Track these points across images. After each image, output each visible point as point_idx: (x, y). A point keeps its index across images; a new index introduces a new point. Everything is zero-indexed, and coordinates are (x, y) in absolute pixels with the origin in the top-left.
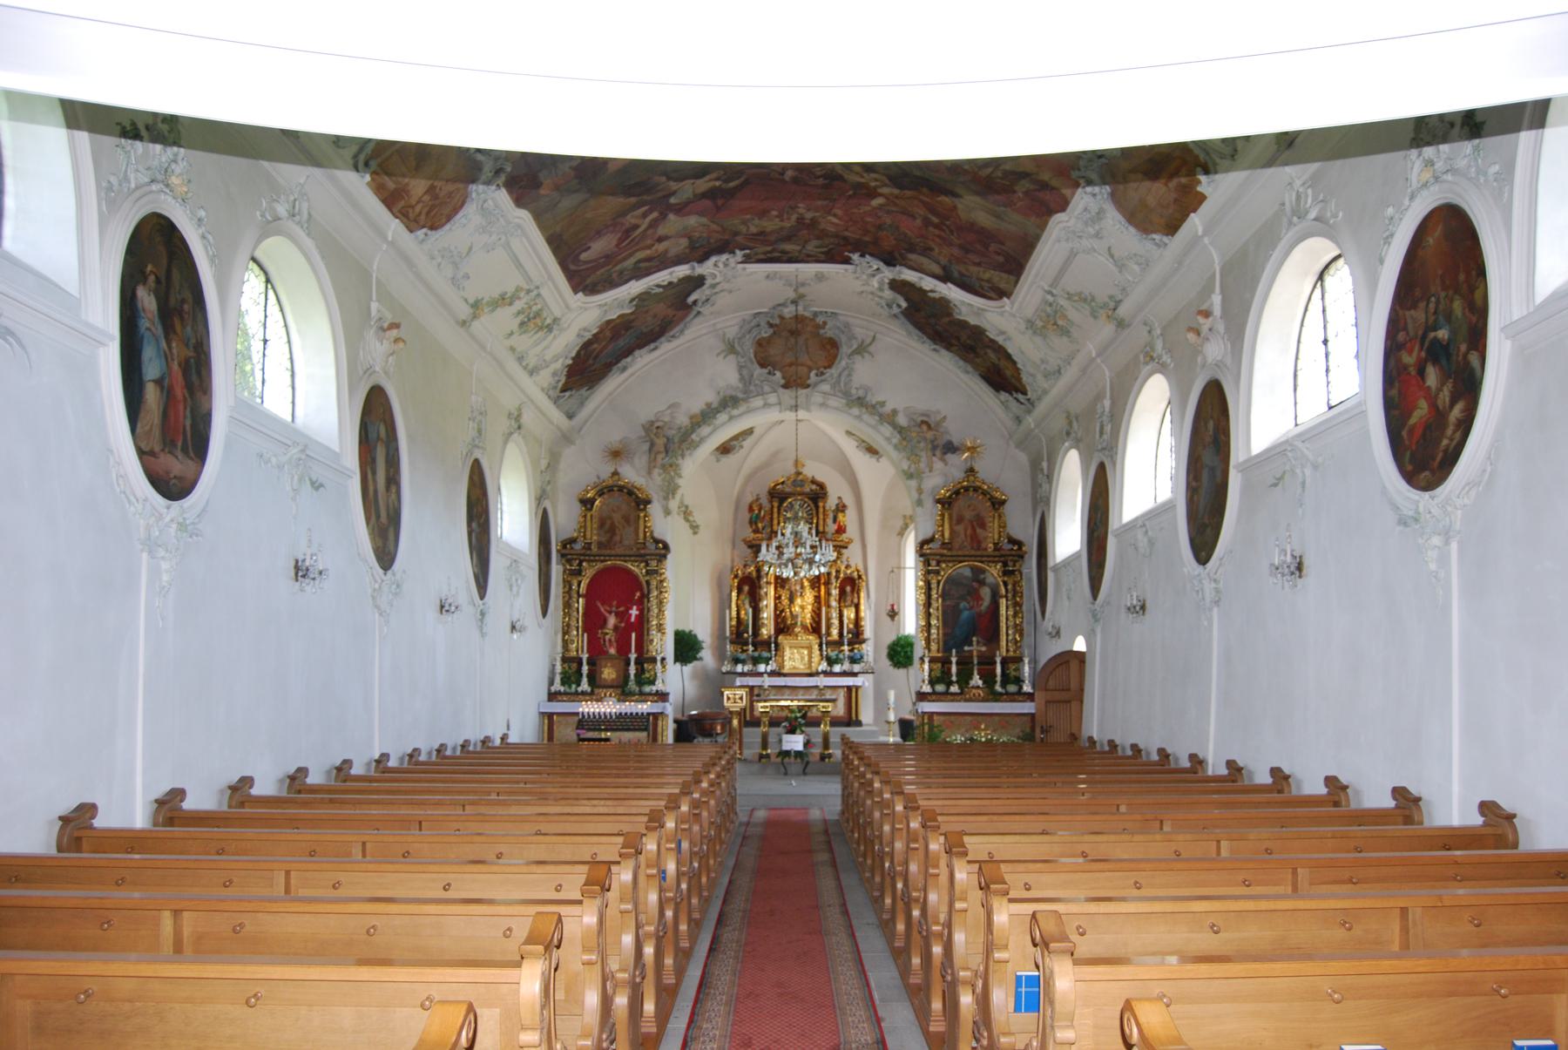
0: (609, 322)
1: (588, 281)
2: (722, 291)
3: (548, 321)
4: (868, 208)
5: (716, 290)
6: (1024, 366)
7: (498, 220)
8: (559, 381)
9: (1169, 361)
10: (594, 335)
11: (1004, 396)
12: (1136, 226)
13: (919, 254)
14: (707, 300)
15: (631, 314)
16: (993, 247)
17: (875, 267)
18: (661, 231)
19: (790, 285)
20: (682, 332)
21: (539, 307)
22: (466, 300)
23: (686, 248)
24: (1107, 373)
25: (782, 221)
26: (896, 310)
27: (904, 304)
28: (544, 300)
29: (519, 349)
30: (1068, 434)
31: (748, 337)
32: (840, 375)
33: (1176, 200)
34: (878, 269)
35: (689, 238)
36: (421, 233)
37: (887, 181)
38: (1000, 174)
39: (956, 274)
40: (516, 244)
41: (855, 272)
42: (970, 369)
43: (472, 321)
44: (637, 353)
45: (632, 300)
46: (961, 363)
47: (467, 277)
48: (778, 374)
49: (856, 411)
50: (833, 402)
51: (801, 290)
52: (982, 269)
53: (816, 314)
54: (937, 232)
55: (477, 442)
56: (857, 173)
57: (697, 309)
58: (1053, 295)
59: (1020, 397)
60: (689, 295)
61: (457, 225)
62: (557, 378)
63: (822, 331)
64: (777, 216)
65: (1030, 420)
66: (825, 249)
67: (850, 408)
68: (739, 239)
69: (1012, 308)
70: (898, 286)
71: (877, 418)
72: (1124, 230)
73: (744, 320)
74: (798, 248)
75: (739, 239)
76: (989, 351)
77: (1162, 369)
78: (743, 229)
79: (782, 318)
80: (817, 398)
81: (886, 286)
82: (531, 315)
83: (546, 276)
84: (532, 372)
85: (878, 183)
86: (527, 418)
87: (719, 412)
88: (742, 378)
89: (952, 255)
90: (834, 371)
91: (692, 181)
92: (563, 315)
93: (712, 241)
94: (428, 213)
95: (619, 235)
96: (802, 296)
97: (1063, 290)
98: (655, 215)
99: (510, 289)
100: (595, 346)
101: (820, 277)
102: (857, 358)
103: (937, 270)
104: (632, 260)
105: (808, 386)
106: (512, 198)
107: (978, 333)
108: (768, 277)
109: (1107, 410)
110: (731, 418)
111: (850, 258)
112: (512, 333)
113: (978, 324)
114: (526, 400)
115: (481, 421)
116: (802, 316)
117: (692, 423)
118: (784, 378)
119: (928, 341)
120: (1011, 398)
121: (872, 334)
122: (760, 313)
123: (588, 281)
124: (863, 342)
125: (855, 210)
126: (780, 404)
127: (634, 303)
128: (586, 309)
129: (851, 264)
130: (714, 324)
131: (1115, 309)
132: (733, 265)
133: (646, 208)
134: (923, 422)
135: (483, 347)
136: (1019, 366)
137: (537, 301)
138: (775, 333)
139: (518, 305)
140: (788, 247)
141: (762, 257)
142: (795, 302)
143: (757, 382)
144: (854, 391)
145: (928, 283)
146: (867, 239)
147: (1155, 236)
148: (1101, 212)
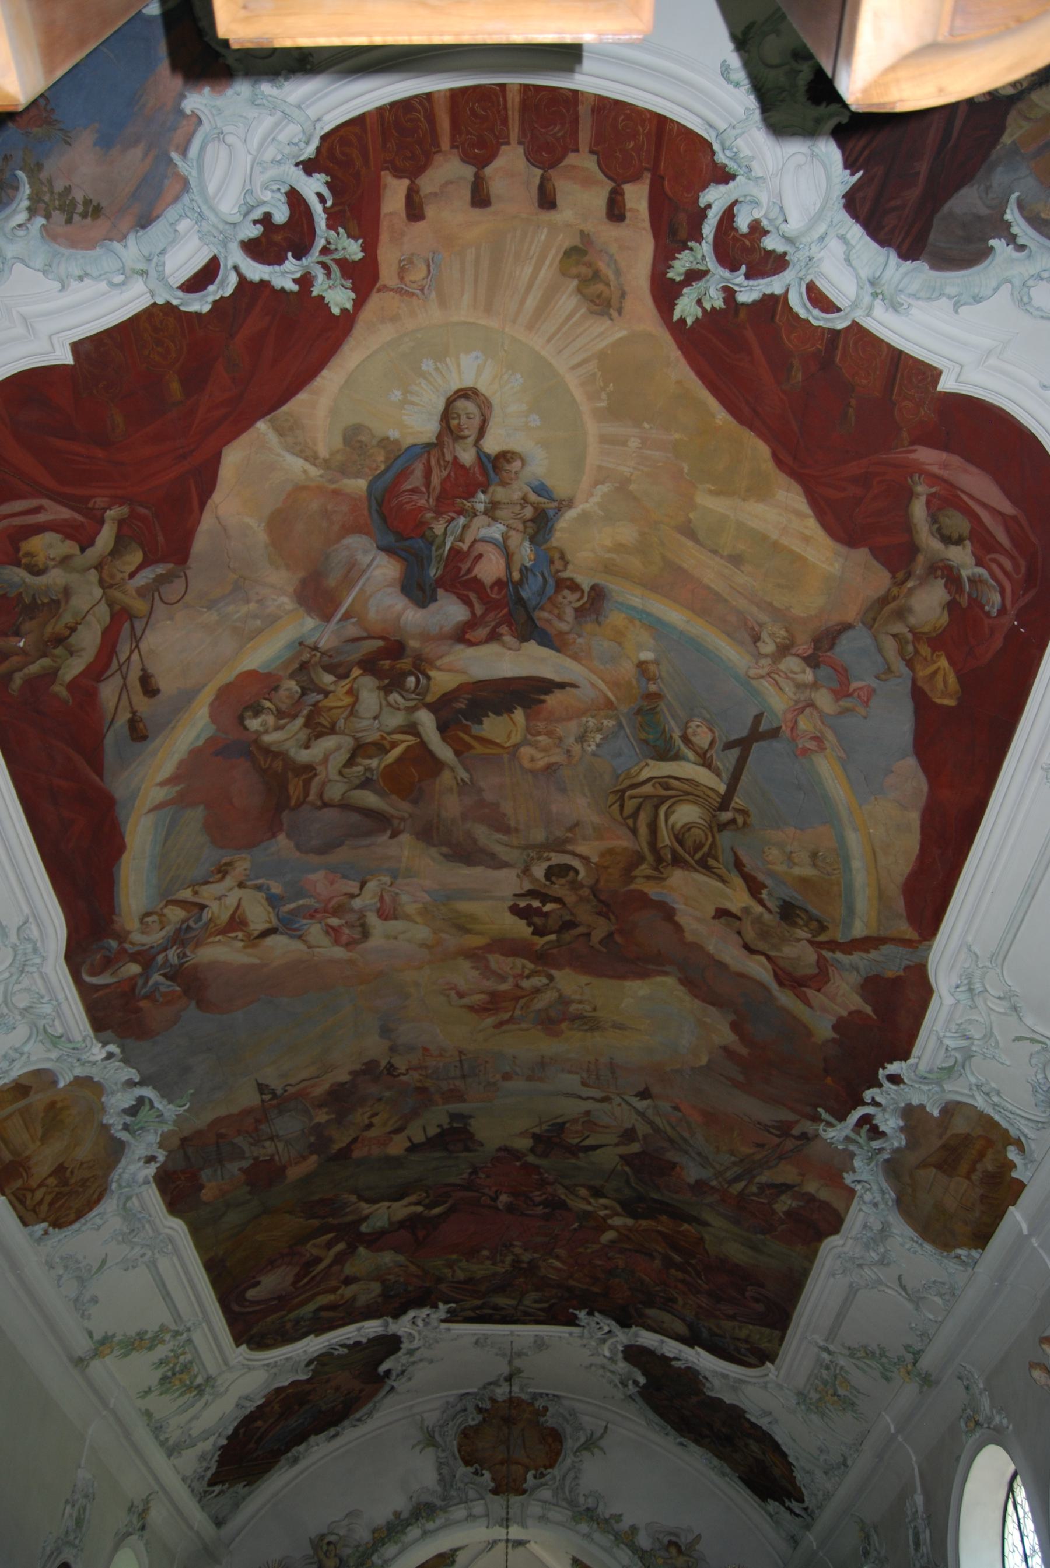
0: (279, 1390)
1: (254, 1330)
2: (421, 1360)
3: (199, 1380)
4: (596, 1247)
5: (412, 1359)
6: (797, 1459)
7: (144, 1227)
8: (208, 1468)
9: (1005, 1421)
10: (259, 1407)
11: (773, 1506)
12: (933, 1242)
13: (660, 1308)
14: (403, 1372)
15: (308, 1381)
17: (606, 1329)
18: (349, 1269)
19: (504, 1355)
20: (370, 1414)
21: (189, 1357)
22: (90, 1334)
23: (379, 1296)
24: (914, 1459)
26: (632, 1389)
27: (642, 1380)
28: (195, 1348)
29: (157, 1416)
30: (866, 1553)
31: (451, 1424)
32: (564, 1478)
33: (983, 1198)
34: (610, 1332)
35: (383, 1282)
36: (40, 1228)
37: (619, 1208)
38: (754, 1189)
39: (705, 1334)
40: (164, 1264)
41: (582, 1337)
42: (728, 1470)
43: (92, 1358)
44: (313, 1439)
45: (310, 1363)
46: (716, 1461)
47: (94, 1300)
48: (487, 1474)
49: (584, 1527)
50: (555, 1514)
51: (517, 1363)
52: (736, 1323)
53: (535, 1397)
54: (680, 1275)
55: (71, 1537)
56: (583, 1199)
57: (390, 1382)
58: (829, 1352)
59: (795, 1506)
60: (381, 1362)
61: (89, 1225)
62: (204, 1464)
63: (542, 1419)
64: (488, 1258)
65: (811, 1538)
66: (546, 1305)
67: (577, 1523)
68: (443, 1287)
69: (777, 1376)
70: (634, 1354)
71: (612, 1537)
72: (919, 1249)
73: (448, 1403)
74: (514, 1302)
75: (443, 1287)
76: (751, 1442)
77: (998, 1437)
78: (448, 1272)
79: (493, 1401)
80: (535, 1509)
81: (620, 1355)
82: (177, 1369)
83: (200, 1315)
84: (172, 1450)
85: (607, 1212)
86: (157, 1515)
87: (409, 1525)
88: (442, 1480)
90: (556, 1472)
91: (387, 1204)
94: (51, 1204)
95: (296, 1269)
96: (519, 1371)
97: (843, 1345)
98: (341, 1246)
99: (152, 1328)
100: (259, 1423)
101: (540, 1344)
102: (586, 1454)
103: (681, 1328)
104: (311, 1307)
105: (524, 1492)
106: (164, 1200)
107: (736, 1414)
108: (477, 1343)
109: (921, 1509)
110: (425, 1534)
111: (576, 1317)
112: (148, 1392)
113: (735, 1402)
114: (156, 1488)
115: (84, 1508)
116: (519, 1398)
117: (374, 1538)
118: (493, 1479)
119: (673, 1432)
120: (783, 1509)
121: (604, 1424)
122: (468, 1394)
123: (254, 1330)
124: (592, 1435)
125: (581, 1250)
126: (487, 1515)
127: (312, 1367)
128: (249, 1369)
129: (578, 1325)
130: (412, 1407)
131: (914, 1364)
132: (435, 1323)
134: (671, 1543)
135: (105, 1405)
136: (791, 1460)
137: (187, 1349)
138: (484, 1419)
139: (162, 1351)
140: (502, 1301)
141: (470, 1314)
142: (509, 1379)
143: (459, 1485)
144: (582, 1500)
145: (671, 1348)
147: (959, 1251)
148: (885, 1228)
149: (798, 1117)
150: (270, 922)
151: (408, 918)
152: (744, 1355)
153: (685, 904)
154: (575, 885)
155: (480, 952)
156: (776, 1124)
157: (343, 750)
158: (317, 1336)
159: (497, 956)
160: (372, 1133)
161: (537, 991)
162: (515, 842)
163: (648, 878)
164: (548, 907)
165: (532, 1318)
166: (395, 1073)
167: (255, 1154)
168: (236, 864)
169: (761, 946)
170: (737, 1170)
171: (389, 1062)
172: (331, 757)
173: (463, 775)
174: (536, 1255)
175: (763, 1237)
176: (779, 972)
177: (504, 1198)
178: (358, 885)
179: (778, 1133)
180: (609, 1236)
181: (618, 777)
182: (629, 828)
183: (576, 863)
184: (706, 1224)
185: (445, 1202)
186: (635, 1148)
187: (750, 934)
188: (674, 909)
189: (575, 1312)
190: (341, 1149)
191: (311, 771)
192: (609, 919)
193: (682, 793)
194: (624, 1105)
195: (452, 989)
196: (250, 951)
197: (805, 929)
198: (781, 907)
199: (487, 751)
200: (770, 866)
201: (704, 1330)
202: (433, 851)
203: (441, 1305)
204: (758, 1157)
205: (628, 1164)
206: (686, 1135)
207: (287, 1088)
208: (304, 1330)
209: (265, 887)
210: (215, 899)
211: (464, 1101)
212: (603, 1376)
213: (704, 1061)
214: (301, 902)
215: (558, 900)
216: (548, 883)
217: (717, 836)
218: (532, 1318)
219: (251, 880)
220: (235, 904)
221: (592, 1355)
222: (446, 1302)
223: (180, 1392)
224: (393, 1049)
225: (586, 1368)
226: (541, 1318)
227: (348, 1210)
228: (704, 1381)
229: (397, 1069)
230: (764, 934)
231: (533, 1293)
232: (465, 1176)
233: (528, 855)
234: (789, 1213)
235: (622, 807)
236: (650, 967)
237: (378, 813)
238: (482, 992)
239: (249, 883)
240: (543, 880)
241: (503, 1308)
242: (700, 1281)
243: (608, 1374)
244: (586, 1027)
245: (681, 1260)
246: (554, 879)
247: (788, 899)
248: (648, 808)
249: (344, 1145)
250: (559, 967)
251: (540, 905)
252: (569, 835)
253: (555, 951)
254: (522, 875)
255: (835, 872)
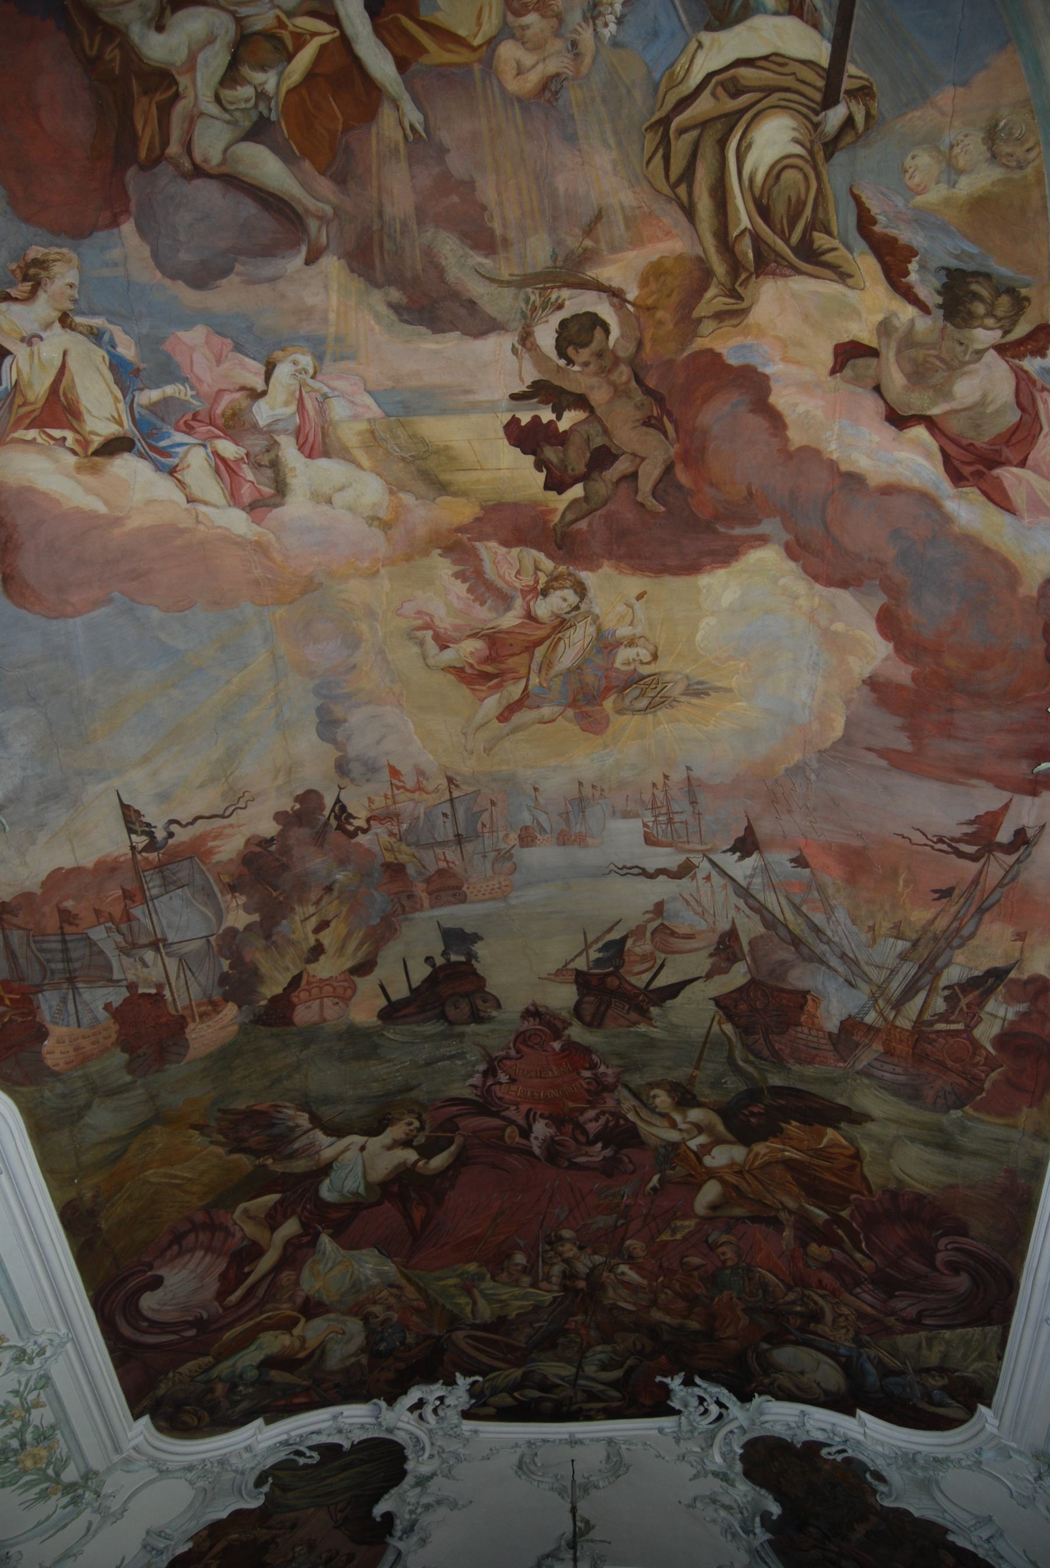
1: (162, 1390)
2: (439, 1502)
3: (70, 1474)
4: (690, 1224)
13: (796, 1343)
16: (945, 1250)
23: (362, 1350)
25: (534, 1285)
27: (775, 1509)
35: (366, 1319)
38: (940, 1004)
45: (260, 1482)
56: (663, 1115)
60: (376, 1499)
64: (525, 1270)
69: (999, 1427)
74: (568, 1371)
81: (739, 1467)
85: (702, 1139)
89: (861, 1315)
91: (358, 1139)
92: (110, 1470)
93: (410, 1339)
111: (667, 1392)
123: (162, 1390)
125: (666, 1237)
127: (266, 1489)
129: (673, 1412)
133: (273, 1198)
140: (555, 1369)
141: (505, 1400)
146: (694, 1325)
149: (1005, 796)
150: (120, 424)
151: (345, 455)
152: (941, 1405)
153: (785, 359)
154: (608, 363)
155: (465, 537)
156: (969, 829)
157: (217, 45)
158: (268, 1422)
159: (493, 544)
160: (325, 969)
161: (562, 624)
162: (505, 275)
163: (720, 316)
164: (568, 420)
165: (601, 1405)
166: (350, 828)
167: (131, 977)
168: (57, 268)
169: (919, 402)
170: (909, 969)
171: (338, 800)
172: (201, 58)
173: (413, 115)
174: (598, 1259)
175: (959, 1113)
176: (952, 450)
177: (541, 1129)
178: (262, 368)
179: (971, 849)
180: (710, 1192)
181: (656, 87)
182: (682, 206)
183: (605, 311)
184: (859, 1118)
185: (450, 1142)
186: (738, 976)
187: (896, 379)
188: (766, 378)
189: (664, 1380)
190: (275, 1000)
191: (169, 87)
192: (665, 434)
193: (759, 95)
194: (716, 878)
195: (427, 627)
196: (87, 478)
197: (990, 322)
198: (945, 290)
199: (448, 57)
200: (919, 200)
201: (869, 1367)
202: (377, 299)
203: (460, 1379)
204: (942, 923)
205: (730, 1018)
206: (819, 918)
207: (174, 828)
208: (245, 1405)
209: (106, 338)
210: (23, 340)
211: (463, 899)
212: (714, 1521)
213: (838, 730)
214: (170, 390)
215: (581, 401)
216: (562, 362)
217: (823, 170)
218: (601, 1405)
219: (83, 314)
220: (58, 363)
221: (696, 1476)
222: (467, 1374)
223: (37, 1489)
224: (342, 768)
225: (688, 1506)
226: (615, 1404)
227: (296, 1146)
228: (875, 1483)
229: (351, 816)
230: (918, 375)
231: (599, 1348)
232: (476, 1080)
233: (527, 300)
234: (1001, 1041)
235: (666, 159)
236: (738, 531)
237: (281, 200)
238: (473, 636)
239: (78, 320)
240: (553, 354)
241: (557, 1386)
242: (858, 1256)
243: (723, 1513)
244: (643, 703)
245: (826, 1216)
246: (570, 351)
247: (954, 264)
248: (708, 150)
249: (279, 990)
250: (592, 564)
251: (553, 417)
252: (588, 243)
253: (583, 525)
254: (519, 347)
255: (1032, 155)
